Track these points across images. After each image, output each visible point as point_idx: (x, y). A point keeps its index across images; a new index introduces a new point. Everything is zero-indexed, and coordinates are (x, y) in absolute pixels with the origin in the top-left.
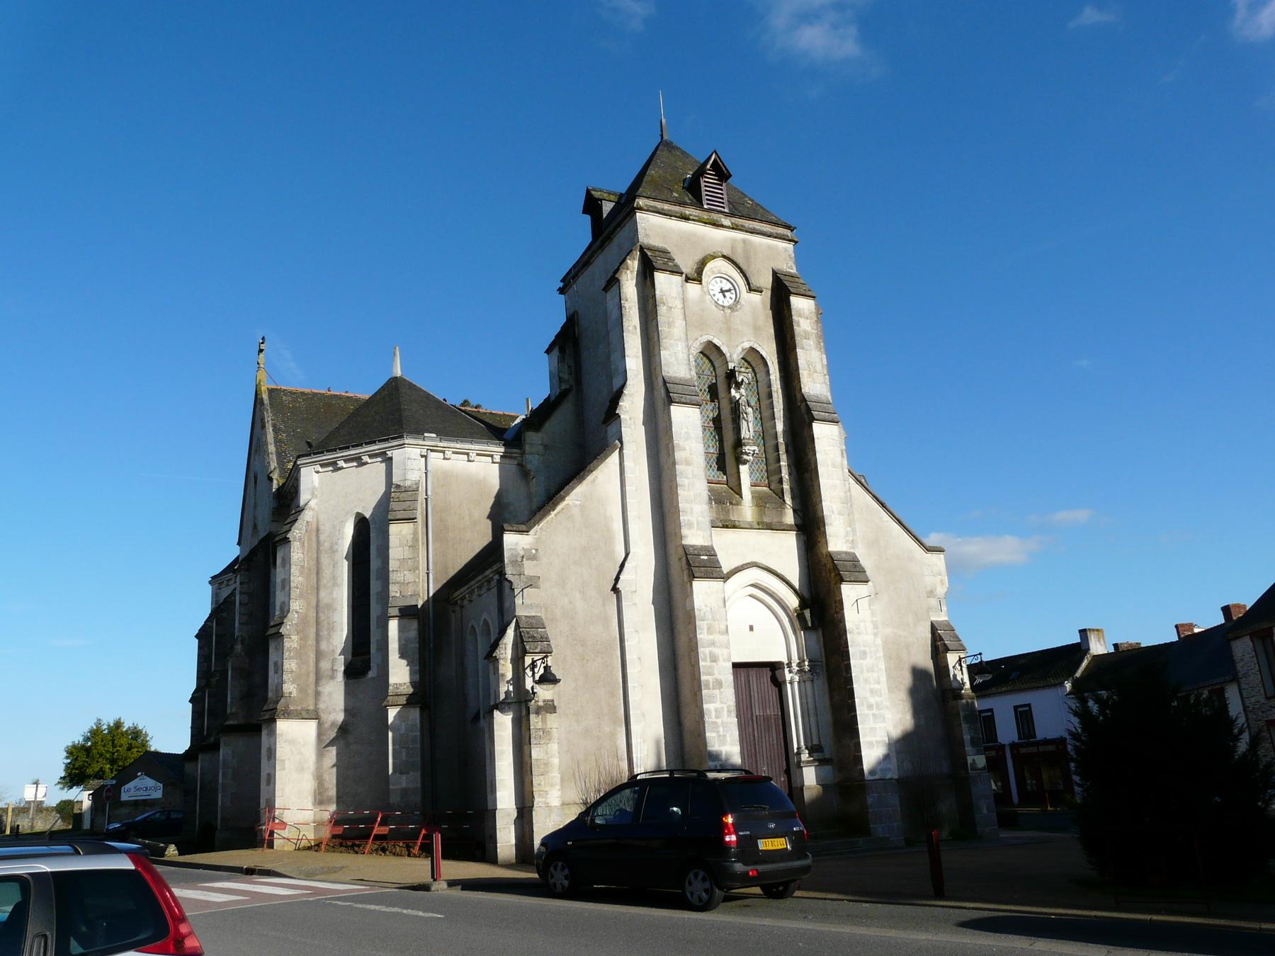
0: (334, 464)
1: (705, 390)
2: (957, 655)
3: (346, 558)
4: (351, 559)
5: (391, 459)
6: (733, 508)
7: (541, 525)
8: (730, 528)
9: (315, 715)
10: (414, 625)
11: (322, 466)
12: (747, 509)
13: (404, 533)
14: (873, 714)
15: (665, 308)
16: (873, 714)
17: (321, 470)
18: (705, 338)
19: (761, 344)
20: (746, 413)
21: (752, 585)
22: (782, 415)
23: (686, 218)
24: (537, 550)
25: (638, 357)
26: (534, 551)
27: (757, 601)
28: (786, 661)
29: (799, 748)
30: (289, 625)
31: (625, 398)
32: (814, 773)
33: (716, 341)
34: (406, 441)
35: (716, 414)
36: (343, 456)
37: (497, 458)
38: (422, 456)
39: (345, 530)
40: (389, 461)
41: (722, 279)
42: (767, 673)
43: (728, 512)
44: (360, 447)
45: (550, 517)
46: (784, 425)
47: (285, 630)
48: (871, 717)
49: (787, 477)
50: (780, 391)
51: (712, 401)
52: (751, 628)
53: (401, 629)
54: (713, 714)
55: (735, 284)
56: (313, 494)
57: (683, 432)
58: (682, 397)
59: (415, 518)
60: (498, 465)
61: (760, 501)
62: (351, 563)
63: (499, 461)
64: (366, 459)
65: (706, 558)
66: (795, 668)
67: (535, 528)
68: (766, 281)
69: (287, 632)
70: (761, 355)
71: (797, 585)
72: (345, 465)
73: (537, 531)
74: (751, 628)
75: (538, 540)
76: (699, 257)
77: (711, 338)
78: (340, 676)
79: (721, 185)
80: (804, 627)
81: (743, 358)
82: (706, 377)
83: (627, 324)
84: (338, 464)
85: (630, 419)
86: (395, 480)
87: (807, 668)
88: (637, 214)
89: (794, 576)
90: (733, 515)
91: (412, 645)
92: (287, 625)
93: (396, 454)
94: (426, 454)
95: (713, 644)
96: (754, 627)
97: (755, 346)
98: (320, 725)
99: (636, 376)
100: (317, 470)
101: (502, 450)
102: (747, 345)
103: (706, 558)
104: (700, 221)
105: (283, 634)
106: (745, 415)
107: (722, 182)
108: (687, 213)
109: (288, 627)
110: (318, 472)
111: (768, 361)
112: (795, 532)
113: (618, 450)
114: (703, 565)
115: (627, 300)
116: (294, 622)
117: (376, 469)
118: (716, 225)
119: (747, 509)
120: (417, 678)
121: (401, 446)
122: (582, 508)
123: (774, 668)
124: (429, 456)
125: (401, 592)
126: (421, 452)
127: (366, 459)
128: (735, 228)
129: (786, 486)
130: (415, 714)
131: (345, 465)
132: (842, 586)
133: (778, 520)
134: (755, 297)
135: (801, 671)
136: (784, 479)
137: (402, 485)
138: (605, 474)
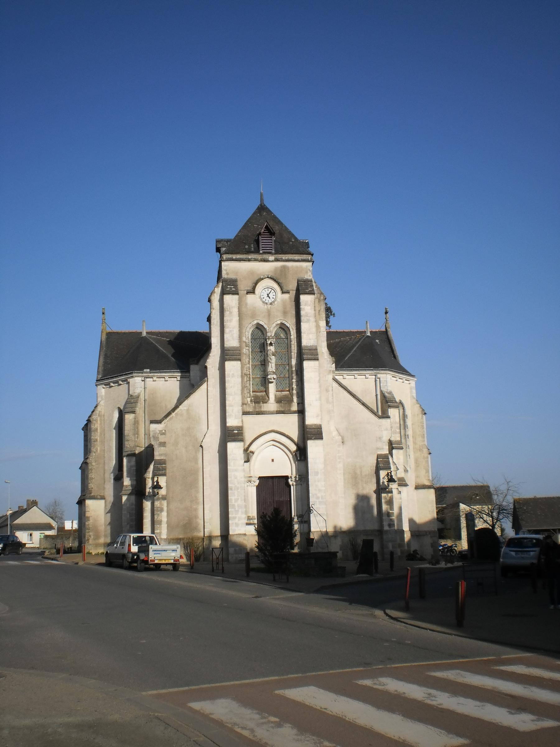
0: (109, 384)
1: (257, 347)
2: (387, 471)
3: (114, 429)
4: (117, 430)
5: (129, 382)
6: (263, 405)
7: (167, 419)
8: (261, 414)
9: (103, 498)
10: (134, 459)
11: (105, 385)
12: (272, 405)
13: (131, 418)
14: (319, 501)
15: (228, 312)
16: (319, 501)
17: (105, 387)
18: (255, 322)
19: (287, 320)
20: (271, 359)
21: (273, 440)
22: (296, 356)
23: (249, 260)
24: (165, 431)
25: (218, 337)
26: (164, 431)
27: (276, 447)
28: (290, 476)
29: (294, 516)
30: (91, 459)
31: (210, 358)
32: (311, 529)
33: (261, 323)
34: (134, 375)
35: (263, 358)
36: (104, 383)
37: (179, 378)
38: (143, 381)
39: (114, 415)
40: (128, 383)
41: (269, 289)
42: (284, 481)
43: (261, 407)
44: (118, 377)
45: (172, 415)
46: (297, 361)
47: (89, 461)
48: (318, 502)
49: (295, 387)
50: (296, 344)
51: (261, 352)
52: (273, 460)
53: (128, 462)
54: (233, 501)
55: (275, 290)
56: (102, 398)
57: (231, 374)
58: (231, 357)
59: (135, 412)
60: (179, 381)
61: (279, 401)
62: (117, 431)
63: (179, 380)
64: (120, 382)
65: (236, 432)
66: (294, 479)
67: (164, 421)
68: (293, 286)
69: (90, 462)
70: (287, 326)
71: (296, 440)
72: (113, 385)
73: (165, 422)
74: (273, 460)
75: (166, 426)
76: (256, 279)
77: (258, 321)
78: (112, 481)
79: (271, 237)
80: (298, 460)
81: (280, 328)
82: (258, 340)
83: (213, 321)
84: (119, 383)
85: (212, 367)
86: (130, 393)
87: (297, 479)
88: (222, 263)
89: (295, 437)
90: (263, 408)
91: (133, 469)
92: (90, 458)
93: (131, 380)
94: (144, 380)
95: (236, 470)
96: (274, 460)
97: (284, 322)
98: (105, 502)
99: (216, 346)
100: (103, 387)
101: (180, 374)
102: (279, 322)
103: (236, 432)
104: (256, 260)
105: (88, 462)
106: (270, 360)
107: (272, 235)
108: (250, 257)
109: (91, 460)
110: (104, 388)
111: (290, 329)
112: (297, 414)
113: (206, 382)
114: (235, 435)
115: (214, 309)
116: (93, 457)
117: (124, 386)
118: (267, 261)
119: (272, 405)
120: (135, 483)
121: (132, 377)
122: (188, 410)
123: (286, 478)
124: (145, 380)
125: (129, 445)
126: (142, 379)
127: (120, 382)
128: (277, 260)
129: (295, 392)
130: (133, 498)
131: (113, 385)
132: (308, 441)
133: (288, 409)
134: (286, 296)
135: (296, 481)
136: (294, 388)
137: (133, 395)
138: (198, 396)
